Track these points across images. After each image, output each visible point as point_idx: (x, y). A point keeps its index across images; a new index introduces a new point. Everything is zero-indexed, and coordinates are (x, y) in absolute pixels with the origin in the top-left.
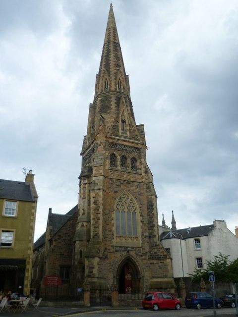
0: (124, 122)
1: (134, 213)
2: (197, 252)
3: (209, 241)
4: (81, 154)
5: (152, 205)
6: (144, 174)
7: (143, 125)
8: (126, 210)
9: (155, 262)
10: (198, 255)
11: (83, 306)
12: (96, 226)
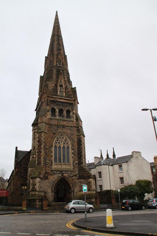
0: (61, 86)
1: (68, 148)
2: (120, 174)
3: (129, 166)
4: (36, 110)
5: (81, 141)
6: (75, 121)
7: (41, 76)
8: (62, 146)
9: (82, 181)
10: (121, 175)
11: (21, 210)
12: (39, 157)
